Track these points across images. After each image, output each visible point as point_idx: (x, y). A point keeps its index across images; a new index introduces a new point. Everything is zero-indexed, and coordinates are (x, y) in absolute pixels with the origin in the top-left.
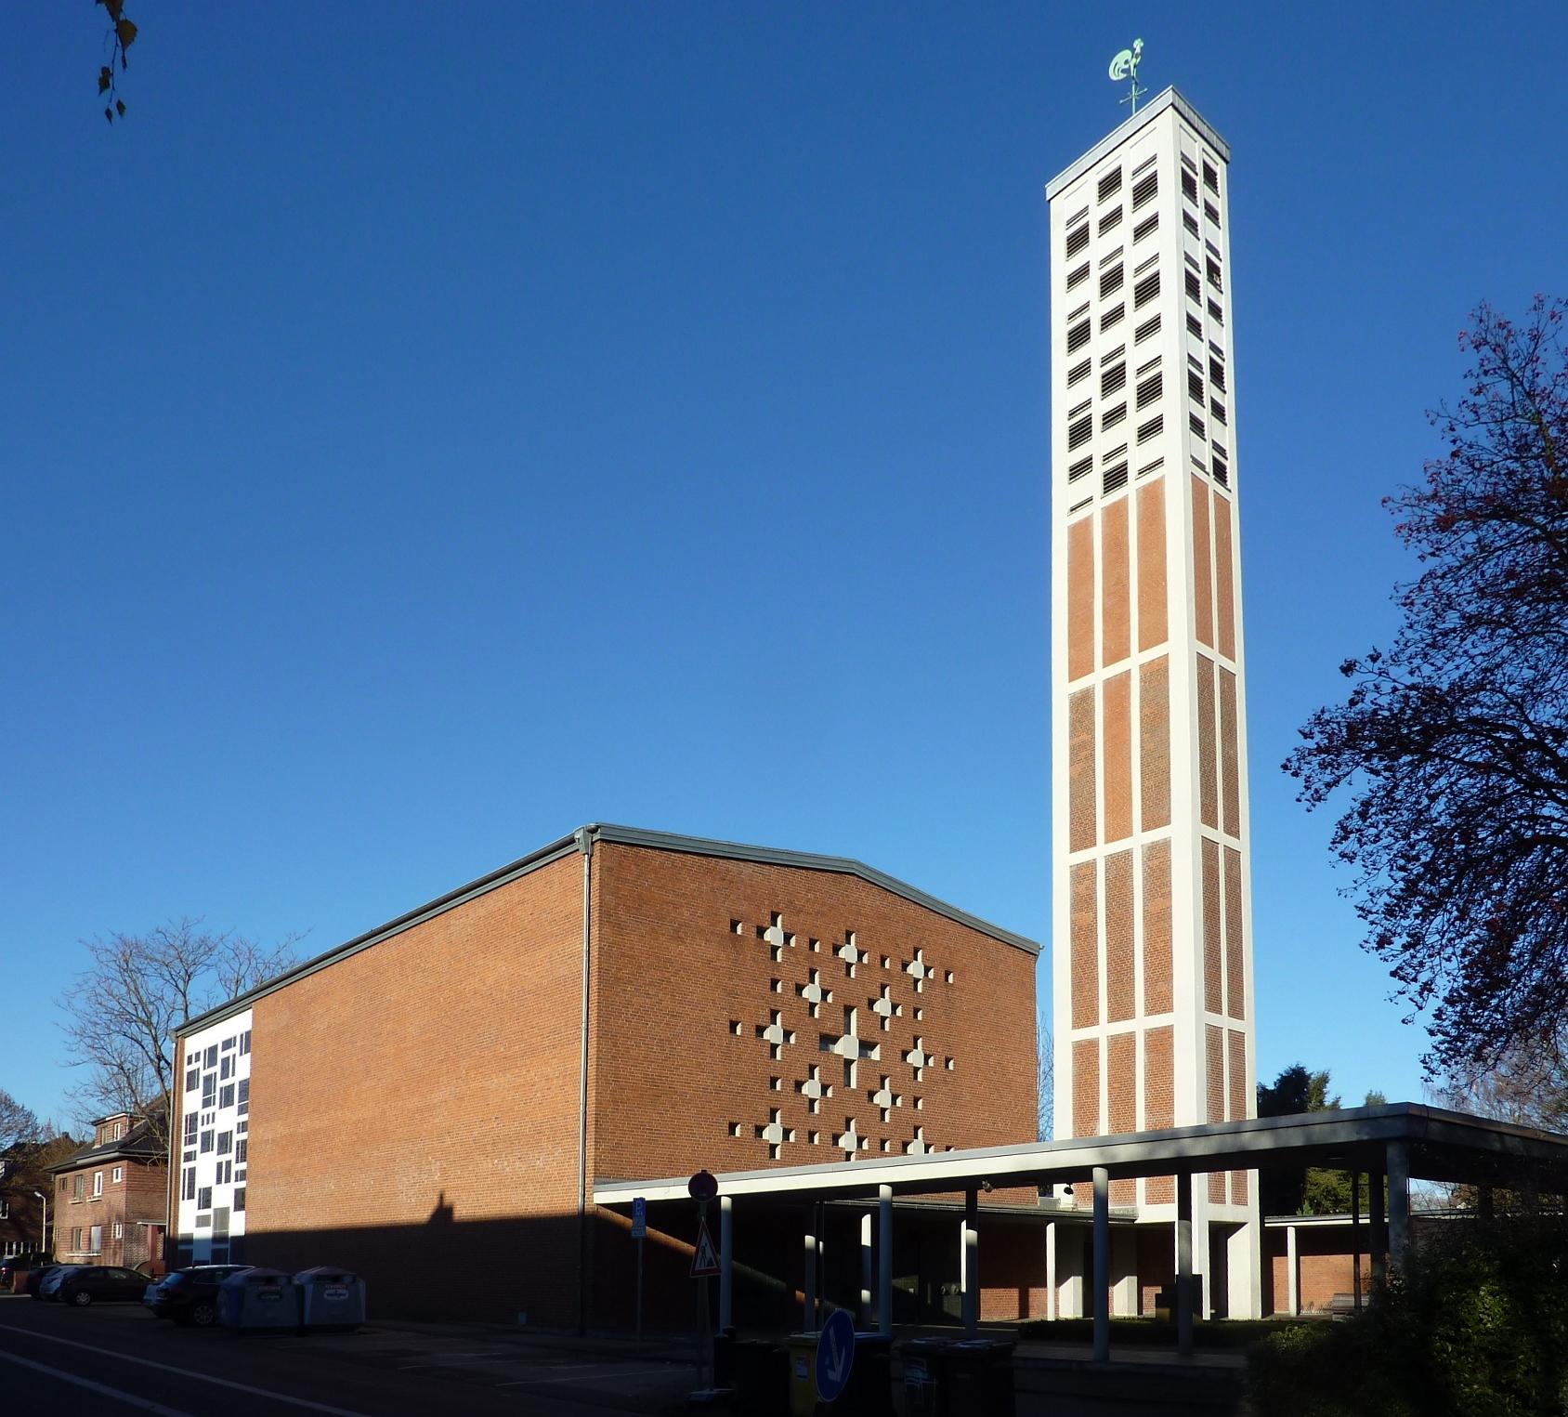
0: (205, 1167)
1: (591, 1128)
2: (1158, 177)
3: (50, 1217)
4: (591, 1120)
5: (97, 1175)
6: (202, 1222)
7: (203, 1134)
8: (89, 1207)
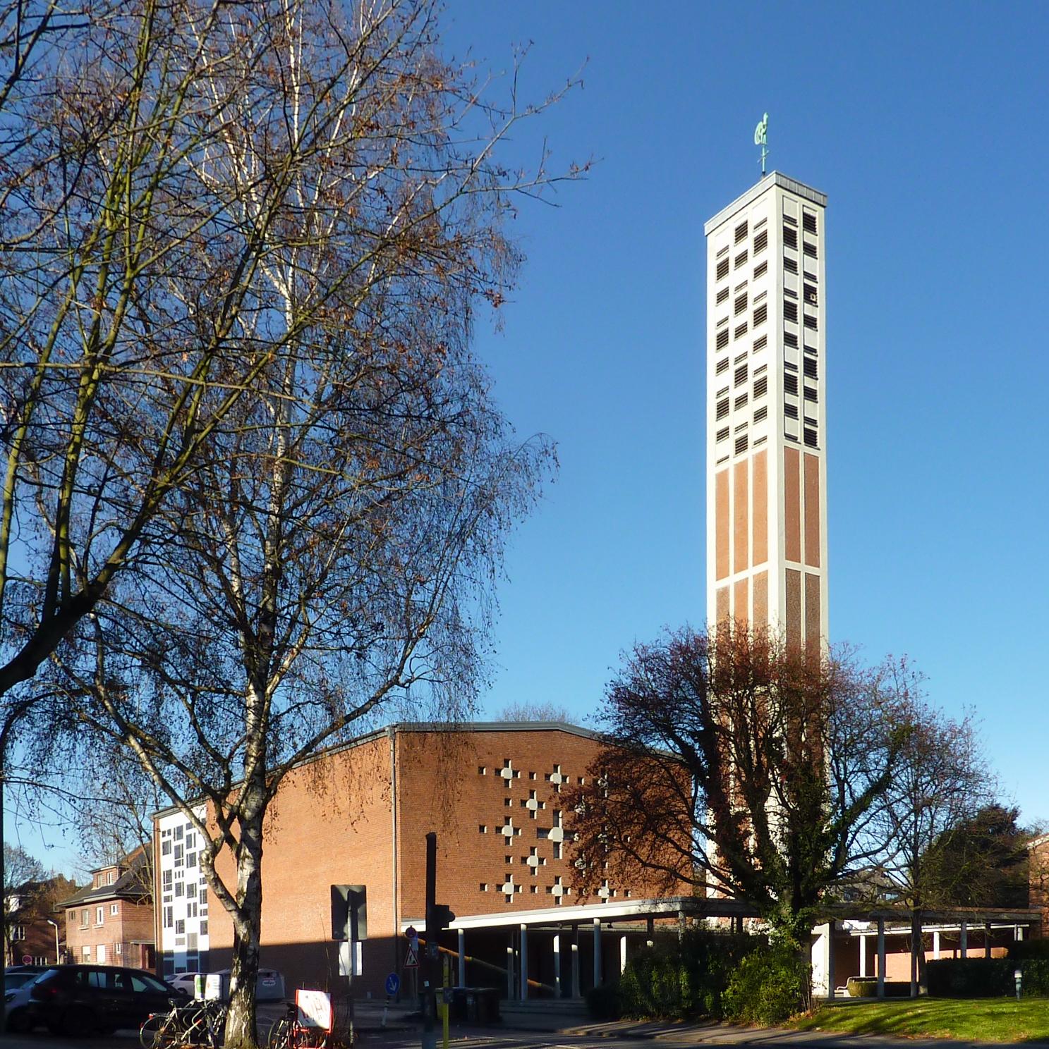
0: (179, 906)
2: (768, 234)
3: (63, 939)
5: (98, 909)
7: (176, 884)
8: (94, 932)
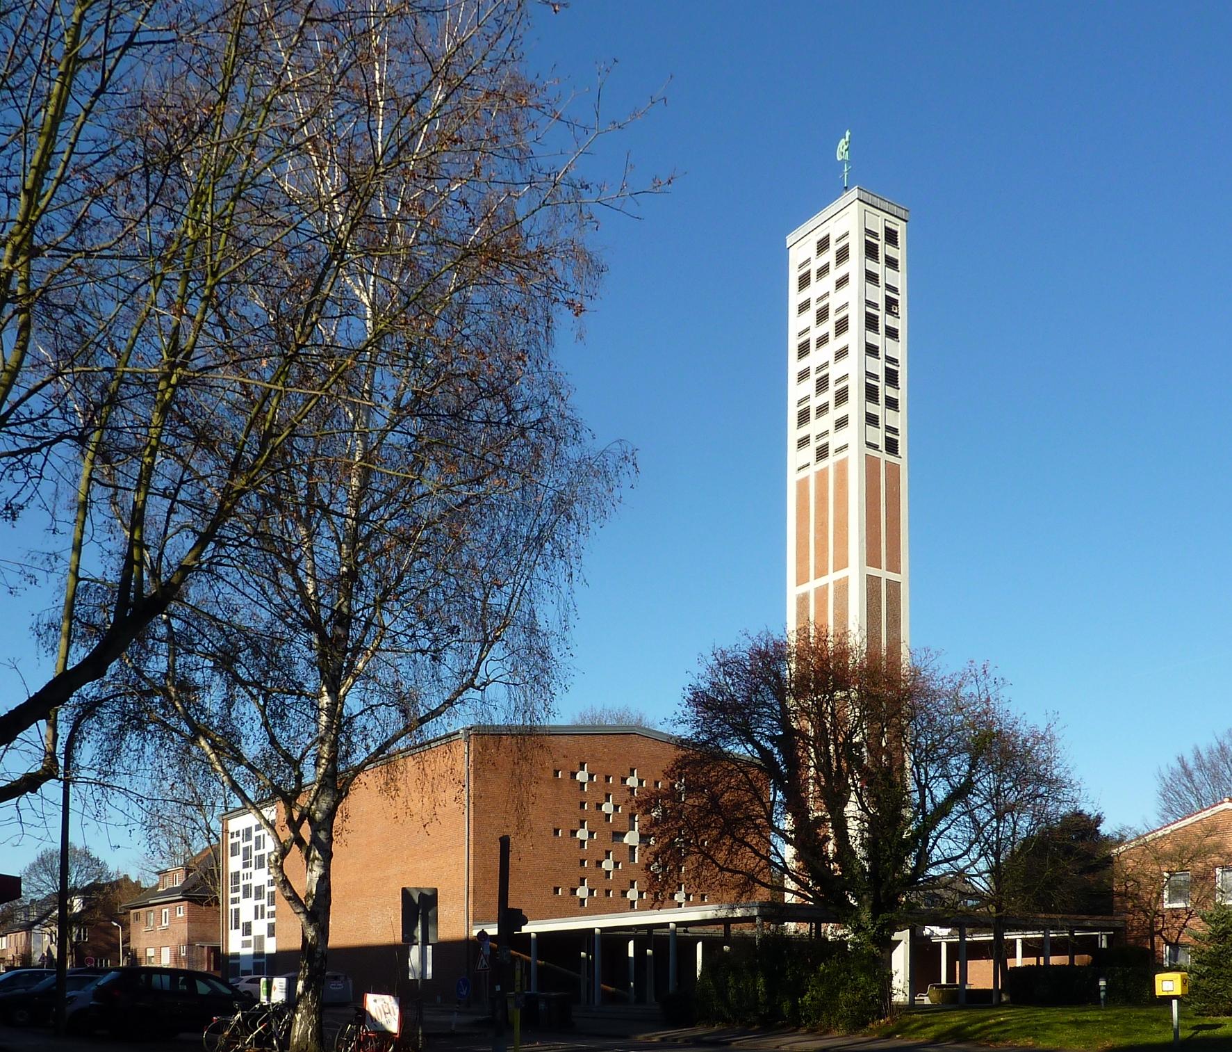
0: (246, 909)
1: (471, 894)
3: (127, 940)
4: (471, 889)
5: (164, 911)
6: (246, 944)
